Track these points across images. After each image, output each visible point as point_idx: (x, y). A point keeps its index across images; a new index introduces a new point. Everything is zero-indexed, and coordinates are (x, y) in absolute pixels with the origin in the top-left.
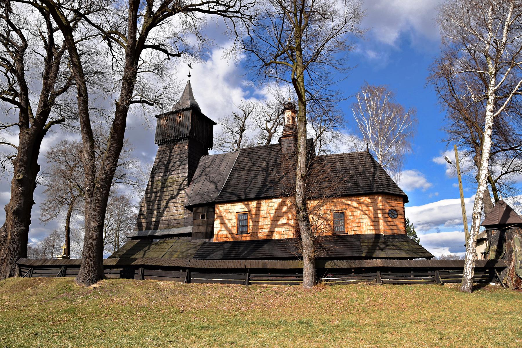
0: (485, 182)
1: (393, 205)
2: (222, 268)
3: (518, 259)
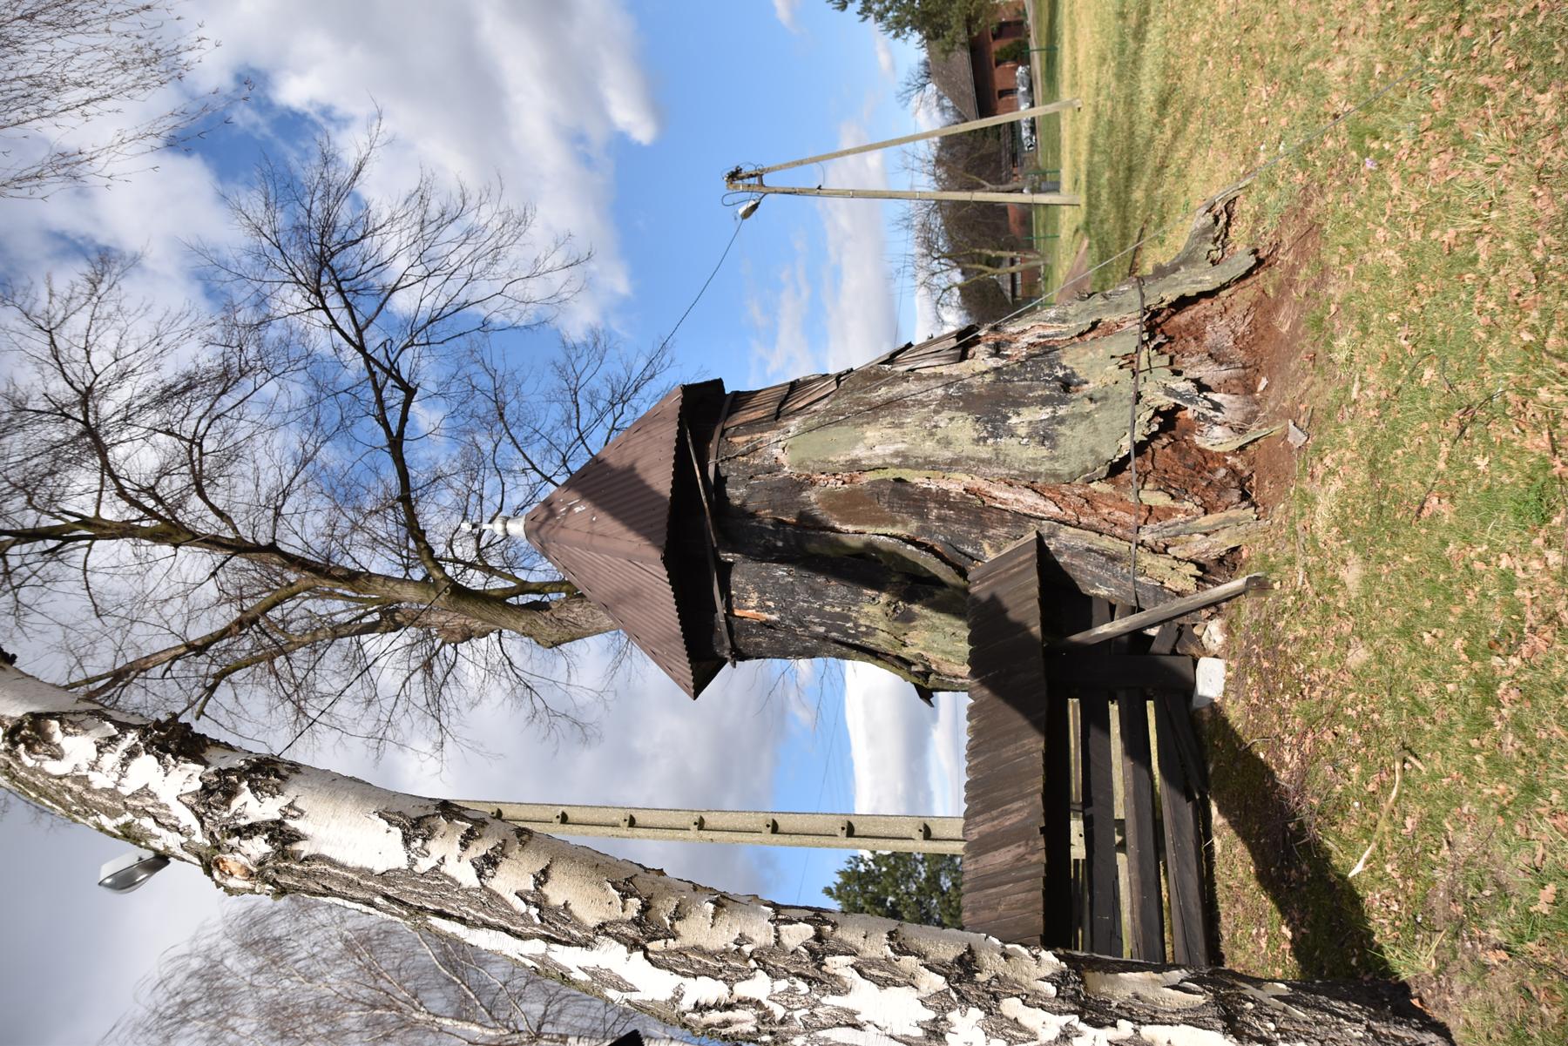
3: (969, 449)
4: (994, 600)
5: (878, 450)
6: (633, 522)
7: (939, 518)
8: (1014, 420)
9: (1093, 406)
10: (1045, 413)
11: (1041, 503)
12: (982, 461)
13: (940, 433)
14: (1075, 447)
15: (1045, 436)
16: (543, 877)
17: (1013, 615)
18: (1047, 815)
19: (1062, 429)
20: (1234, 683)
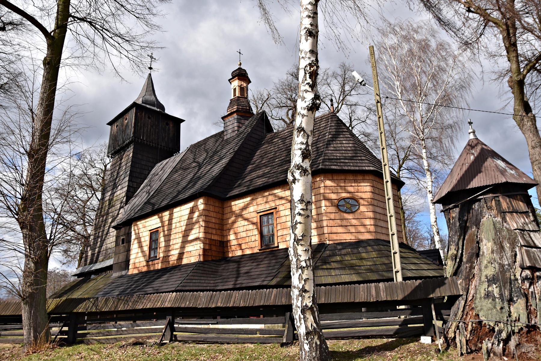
0: (307, 88)
1: (351, 189)
2: (242, 305)
3: (484, 274)
4: (445, 284)
5: (485, 247)
6: (460, 182)
7: (466, 267)
8: (494, 286)
9: (498, 309)
10: (497, 295)
11: (471, 295)
12: (480, 278)
13: (489, 265)
14: (484, 304)
15: (488, 295)
16: (300, 223)
17: (438, 290)
18: (381, 301)
19: (490, 300)
20: (422, 346)
